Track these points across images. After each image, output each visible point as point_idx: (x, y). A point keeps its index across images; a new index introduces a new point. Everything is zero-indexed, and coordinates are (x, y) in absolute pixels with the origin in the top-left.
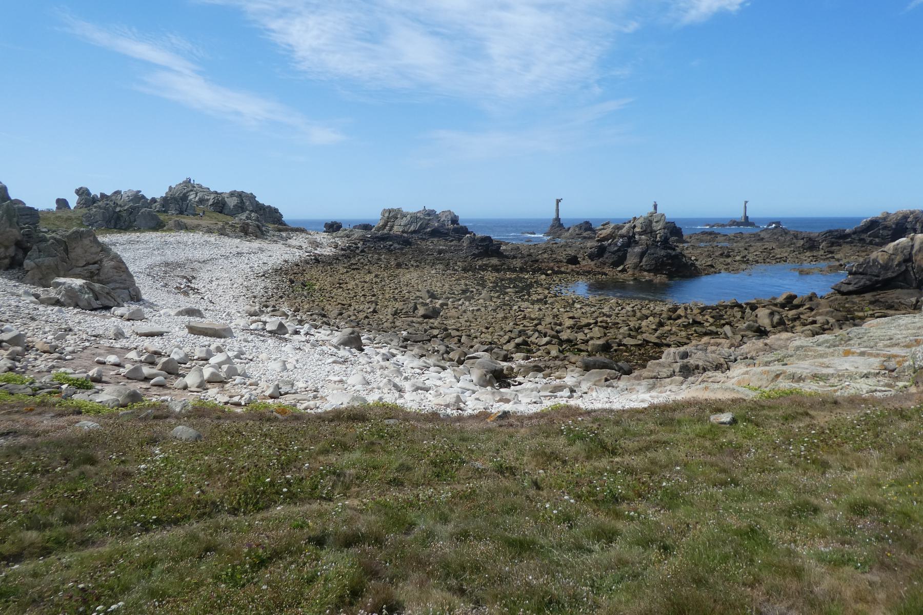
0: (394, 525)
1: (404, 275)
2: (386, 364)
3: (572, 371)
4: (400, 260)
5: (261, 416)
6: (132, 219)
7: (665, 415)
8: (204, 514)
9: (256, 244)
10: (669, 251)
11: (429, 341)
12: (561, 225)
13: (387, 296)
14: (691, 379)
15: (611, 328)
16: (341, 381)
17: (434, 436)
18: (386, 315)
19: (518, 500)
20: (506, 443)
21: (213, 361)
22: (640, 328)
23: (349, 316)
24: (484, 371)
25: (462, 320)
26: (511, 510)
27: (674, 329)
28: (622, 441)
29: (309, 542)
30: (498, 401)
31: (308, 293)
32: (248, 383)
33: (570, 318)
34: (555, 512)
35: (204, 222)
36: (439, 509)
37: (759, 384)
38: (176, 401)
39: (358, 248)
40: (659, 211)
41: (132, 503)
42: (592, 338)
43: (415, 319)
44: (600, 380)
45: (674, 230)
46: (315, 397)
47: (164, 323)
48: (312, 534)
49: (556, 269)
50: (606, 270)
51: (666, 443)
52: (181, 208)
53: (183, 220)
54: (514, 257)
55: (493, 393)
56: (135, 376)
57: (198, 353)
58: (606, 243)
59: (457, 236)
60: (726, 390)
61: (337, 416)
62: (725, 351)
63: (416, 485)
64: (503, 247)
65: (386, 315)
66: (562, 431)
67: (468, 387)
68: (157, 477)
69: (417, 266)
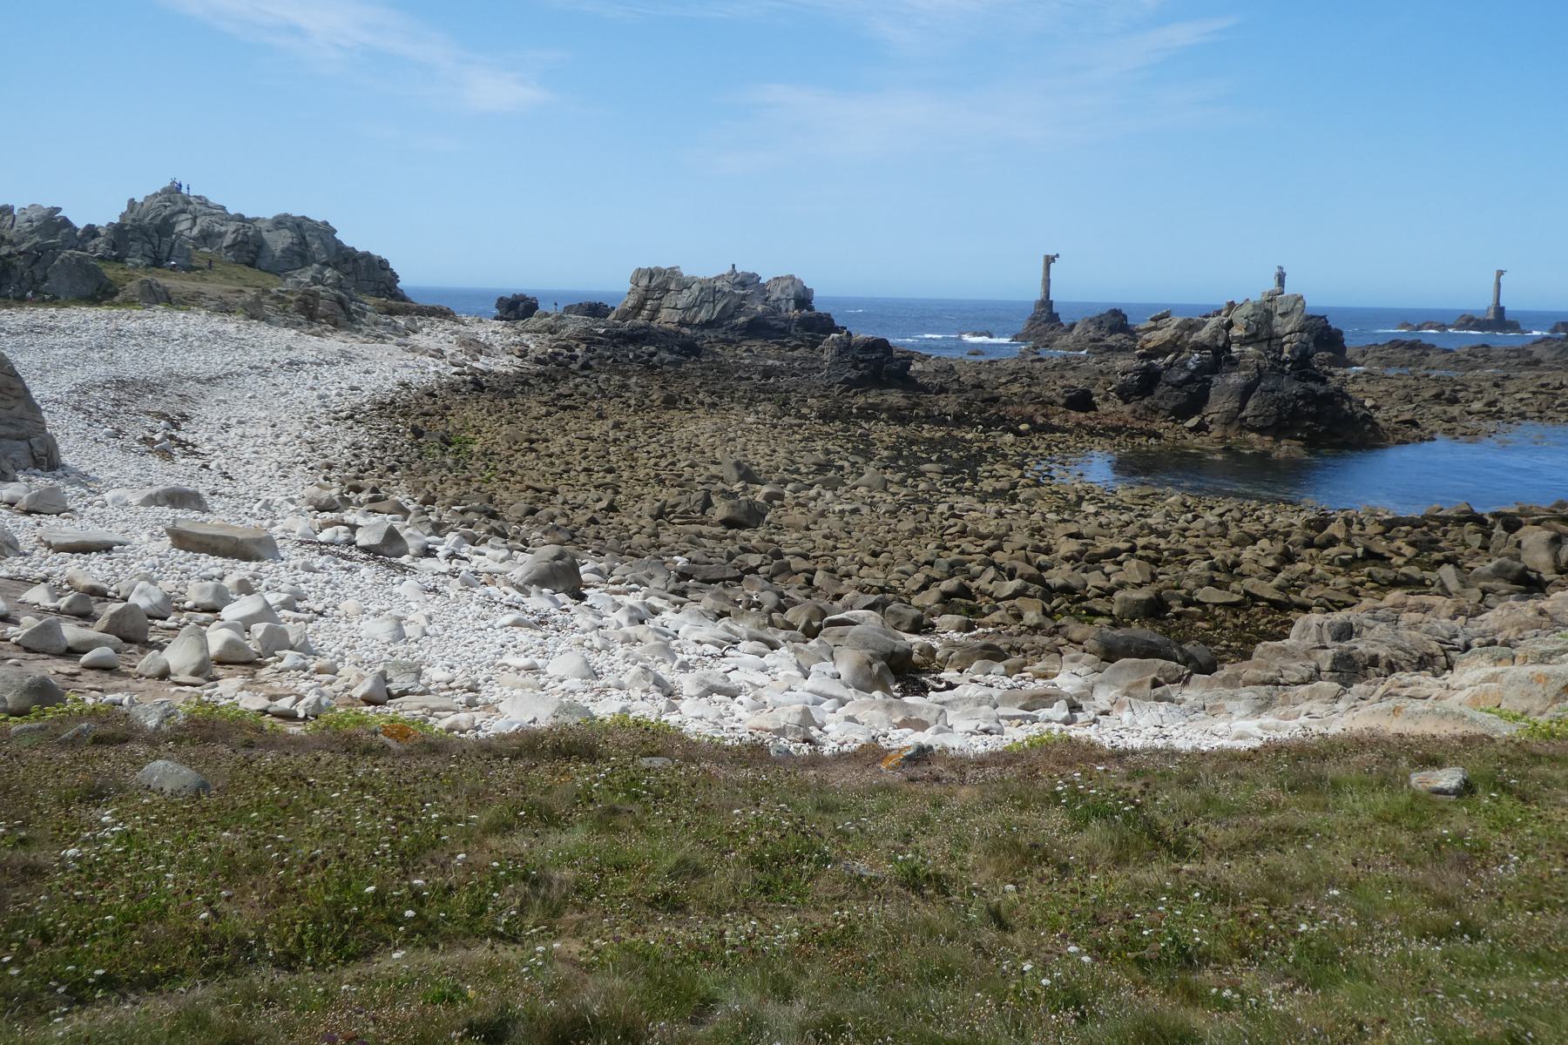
0: (667, 1000)
1: (681, 424)
2: (638, 630)
3: (1074, 660)
4: (674, 390)
5: (352, 744)
6: (39, 275)
7: (1303, 767)
8: (218, 966)
9: (334, 343)
10: (1311, 385)
11: (739, 579)
12: (1053, 318)
13: (641, 473)
14: (1358, 688)
15: (1168, 562)
16: (532, 669)
17: (756, 798)
18: (637, 517)
19: (958, 952)
20: (925, 820)
21: (230, 613)
22: (1236, 564)
23: (552, 518)
24: (867, 654)
25: (817, 535)
26: (941, 975)
27: (1319, 570)
28: (1199, 827)
29: (470, 1034)
30: (899, 726)
31: (456, 462)
32: (313, 667)
33: (1071, 536)
34: (1045, 982)
35: (213, 287)
36: (771, 968)
37: (1525, 705)
38: (149, 707)
39: (574, 358)
40: (1288, 291)
41: (46, 939)
42: (1121, 586)
43: (705, 529)
44: (1140, 684)
45: (1324, 335)
46: (471, 704)
47: (114, 520)
48: (477, 1016)
49: (1040, 420)
50: (1159, 425)
51: (1303, 833)
52: (155, 253)
53: (161, 281)
54: (942, 390)
55: (888, 706)
56: (42, 644)
57: (196, 593)
58: (1159, 362)
59: (807, 335)
60: (1443, 716)
61: (529, 747)
62: (1443, 624)
63: (715, 910)
64: (916, 366)
65: (637, 517)
66: (1056, 795)
67: (828, 691)
68: (107, 879)
69: (714, 405)
